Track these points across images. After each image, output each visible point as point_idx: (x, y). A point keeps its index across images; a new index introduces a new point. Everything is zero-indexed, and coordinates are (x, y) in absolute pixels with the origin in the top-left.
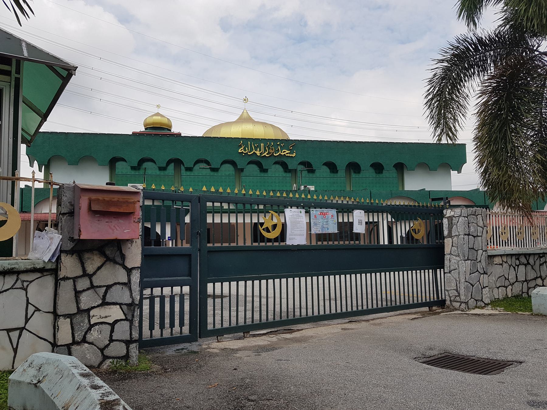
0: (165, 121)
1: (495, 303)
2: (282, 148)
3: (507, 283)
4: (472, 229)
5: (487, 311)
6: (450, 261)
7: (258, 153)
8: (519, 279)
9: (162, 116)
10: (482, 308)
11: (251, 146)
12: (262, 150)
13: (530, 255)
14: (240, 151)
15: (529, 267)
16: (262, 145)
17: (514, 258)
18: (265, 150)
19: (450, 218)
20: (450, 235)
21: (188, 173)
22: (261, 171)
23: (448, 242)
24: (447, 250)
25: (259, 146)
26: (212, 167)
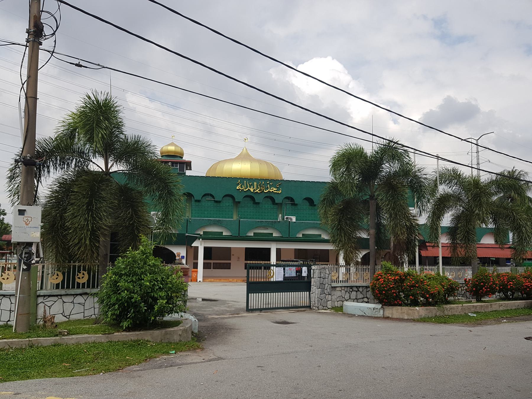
0: (179, 150)
1: (332, 308)
2: (271, 186)
3: (343, 299)
4: (322, 275)
5: (328, 311)
6: (313, 288)
7: (252, 190)
8: (351, 298)
9: (176, 146)
10: (326, 310)
11: (246, 184)
12: (255, 187)
13: (360, 287)
14: (237, 188)
15: (359, 293)
16: (255, 183)
17: (349, 288)
18: (257, 188)
19: (314, 270)
20: (313, 278)
21: (197, 203)
22: (254, 203)
23: (312, 280)
24: (312, 284)
25: (253, 185)
26: (216, 200)
